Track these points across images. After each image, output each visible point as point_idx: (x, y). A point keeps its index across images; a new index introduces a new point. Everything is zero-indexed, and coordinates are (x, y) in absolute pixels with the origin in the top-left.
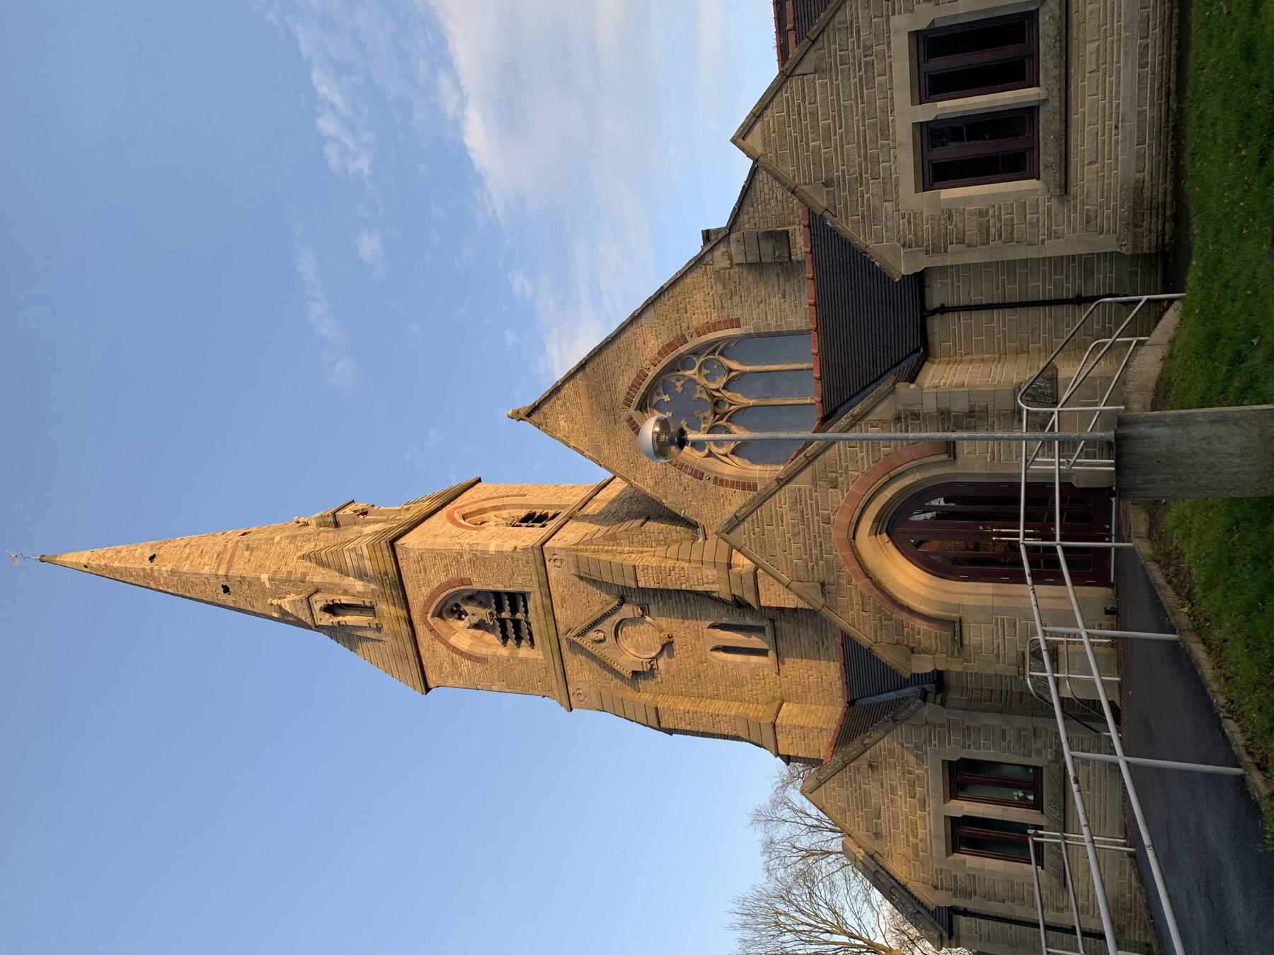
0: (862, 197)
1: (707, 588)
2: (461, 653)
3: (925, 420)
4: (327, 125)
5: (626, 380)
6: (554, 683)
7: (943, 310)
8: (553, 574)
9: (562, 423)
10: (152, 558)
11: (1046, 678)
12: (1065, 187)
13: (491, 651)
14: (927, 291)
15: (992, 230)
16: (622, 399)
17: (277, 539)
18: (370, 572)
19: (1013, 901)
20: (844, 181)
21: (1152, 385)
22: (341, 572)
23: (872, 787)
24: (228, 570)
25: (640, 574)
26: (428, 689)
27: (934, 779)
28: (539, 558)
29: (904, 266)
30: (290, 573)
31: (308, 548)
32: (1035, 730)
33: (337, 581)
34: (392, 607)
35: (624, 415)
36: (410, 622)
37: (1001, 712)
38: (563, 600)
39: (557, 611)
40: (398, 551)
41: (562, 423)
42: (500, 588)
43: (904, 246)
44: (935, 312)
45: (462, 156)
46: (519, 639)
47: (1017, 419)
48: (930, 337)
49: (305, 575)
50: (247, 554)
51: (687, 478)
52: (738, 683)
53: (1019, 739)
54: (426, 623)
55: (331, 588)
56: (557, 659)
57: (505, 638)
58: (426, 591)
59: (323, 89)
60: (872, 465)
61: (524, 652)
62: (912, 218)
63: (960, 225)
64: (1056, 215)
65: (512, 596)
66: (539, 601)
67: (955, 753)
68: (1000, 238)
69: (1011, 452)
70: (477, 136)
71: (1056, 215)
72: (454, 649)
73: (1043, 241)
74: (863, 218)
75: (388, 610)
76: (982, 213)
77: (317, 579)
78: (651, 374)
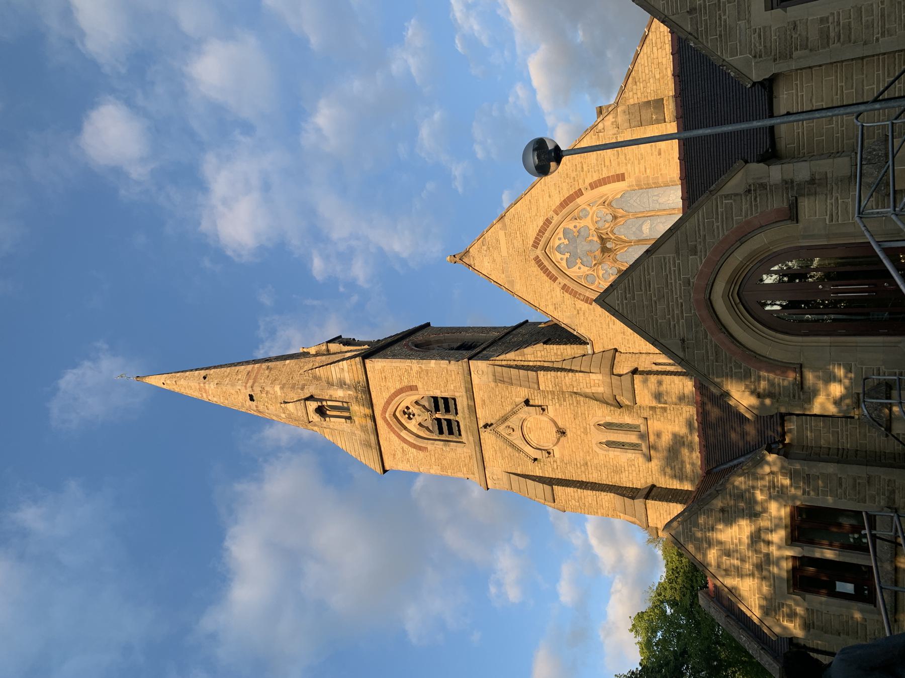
0: (720, 19)
1: (594, 390)
3: (771, 190)
5: (535, 226)
6: (476, 468)
9: (486, 264)
15: (832, 34)
16: (531, 243)
18: (348, 381)
19: (848, 634)
20: (705, 7)
29: (757, 74)
32: (869, 479)
34: (362, 408)
36: (374, 419)
37: (838, 462)
41: (486, 264)
42: (438, 394)
43: (755, 57)
46: (451, 432)
47: (853, 182)
48: (777, 140)
50: (267, 372)
53: (854, 486)
56: (478, 449)
57: (441, 432)
58: (386, 395)
60: (726, 233)
63: (804, 34)
64: (889, 16)
66: (465, 403)
68: (839, 40)
69: (847, 212)
71: (889, 16)
73: (877, 39)
74: (720, 36)
75: (358, 410)
76: (823, 20)
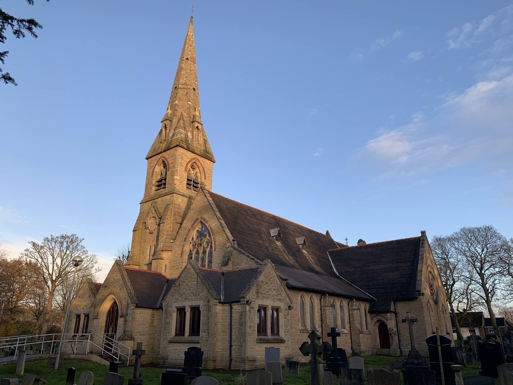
2: (154, 169)
4: (467, 27)
7: (231, 308)
8: (168, 197)
10: (187, 59)
11: (52, 340)
12: (170, 342)
13: (154, 178)
14: (236, 304)
17: (189, 103)
21: (90, 359)
22: (176, 128)
23: (87, 296)
24: (180, 88)
25: (163, 224)
26: (147, 159)
27: (86, 311)
28: (171, 192)
30: (177, 110)
31: (185, 115)
33: (173, 127)
35: (199, 217)
38: (162, 200)
39: (160, 199)
40: (176, 148)
44: (231, 306)
45: (472, 83)
46: (158, 186)
49: (176, 116)
50: (185, 93)
51: (185, 236)
52: (143, 252)
54: (161, 158)
55: (171, 125)
57: (159, 182)
58: (167, 157)
59: (485, 21)
61: (154, 188)
62: (171, 306)
65: (165, 184)
66: (163, 193)
67: (201, 309)
70: (484, 87)
72: (155, 167)
77: (174, 120)
78: (207, 225)
